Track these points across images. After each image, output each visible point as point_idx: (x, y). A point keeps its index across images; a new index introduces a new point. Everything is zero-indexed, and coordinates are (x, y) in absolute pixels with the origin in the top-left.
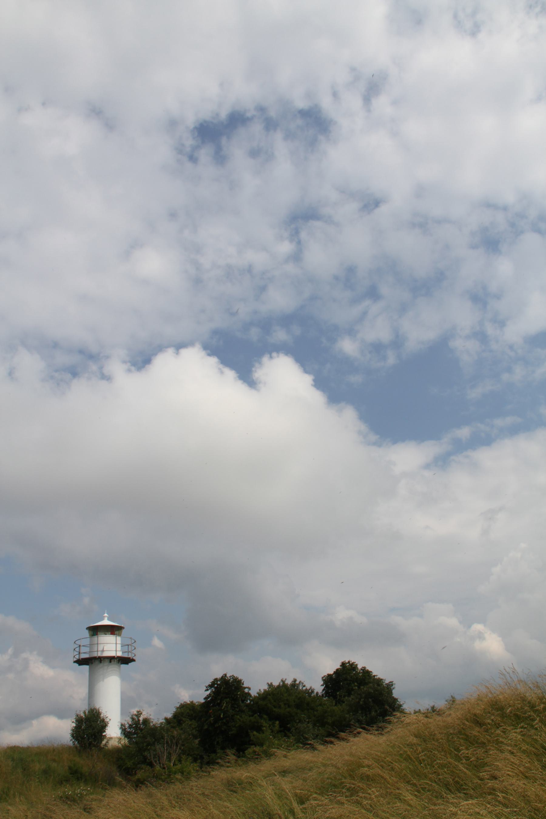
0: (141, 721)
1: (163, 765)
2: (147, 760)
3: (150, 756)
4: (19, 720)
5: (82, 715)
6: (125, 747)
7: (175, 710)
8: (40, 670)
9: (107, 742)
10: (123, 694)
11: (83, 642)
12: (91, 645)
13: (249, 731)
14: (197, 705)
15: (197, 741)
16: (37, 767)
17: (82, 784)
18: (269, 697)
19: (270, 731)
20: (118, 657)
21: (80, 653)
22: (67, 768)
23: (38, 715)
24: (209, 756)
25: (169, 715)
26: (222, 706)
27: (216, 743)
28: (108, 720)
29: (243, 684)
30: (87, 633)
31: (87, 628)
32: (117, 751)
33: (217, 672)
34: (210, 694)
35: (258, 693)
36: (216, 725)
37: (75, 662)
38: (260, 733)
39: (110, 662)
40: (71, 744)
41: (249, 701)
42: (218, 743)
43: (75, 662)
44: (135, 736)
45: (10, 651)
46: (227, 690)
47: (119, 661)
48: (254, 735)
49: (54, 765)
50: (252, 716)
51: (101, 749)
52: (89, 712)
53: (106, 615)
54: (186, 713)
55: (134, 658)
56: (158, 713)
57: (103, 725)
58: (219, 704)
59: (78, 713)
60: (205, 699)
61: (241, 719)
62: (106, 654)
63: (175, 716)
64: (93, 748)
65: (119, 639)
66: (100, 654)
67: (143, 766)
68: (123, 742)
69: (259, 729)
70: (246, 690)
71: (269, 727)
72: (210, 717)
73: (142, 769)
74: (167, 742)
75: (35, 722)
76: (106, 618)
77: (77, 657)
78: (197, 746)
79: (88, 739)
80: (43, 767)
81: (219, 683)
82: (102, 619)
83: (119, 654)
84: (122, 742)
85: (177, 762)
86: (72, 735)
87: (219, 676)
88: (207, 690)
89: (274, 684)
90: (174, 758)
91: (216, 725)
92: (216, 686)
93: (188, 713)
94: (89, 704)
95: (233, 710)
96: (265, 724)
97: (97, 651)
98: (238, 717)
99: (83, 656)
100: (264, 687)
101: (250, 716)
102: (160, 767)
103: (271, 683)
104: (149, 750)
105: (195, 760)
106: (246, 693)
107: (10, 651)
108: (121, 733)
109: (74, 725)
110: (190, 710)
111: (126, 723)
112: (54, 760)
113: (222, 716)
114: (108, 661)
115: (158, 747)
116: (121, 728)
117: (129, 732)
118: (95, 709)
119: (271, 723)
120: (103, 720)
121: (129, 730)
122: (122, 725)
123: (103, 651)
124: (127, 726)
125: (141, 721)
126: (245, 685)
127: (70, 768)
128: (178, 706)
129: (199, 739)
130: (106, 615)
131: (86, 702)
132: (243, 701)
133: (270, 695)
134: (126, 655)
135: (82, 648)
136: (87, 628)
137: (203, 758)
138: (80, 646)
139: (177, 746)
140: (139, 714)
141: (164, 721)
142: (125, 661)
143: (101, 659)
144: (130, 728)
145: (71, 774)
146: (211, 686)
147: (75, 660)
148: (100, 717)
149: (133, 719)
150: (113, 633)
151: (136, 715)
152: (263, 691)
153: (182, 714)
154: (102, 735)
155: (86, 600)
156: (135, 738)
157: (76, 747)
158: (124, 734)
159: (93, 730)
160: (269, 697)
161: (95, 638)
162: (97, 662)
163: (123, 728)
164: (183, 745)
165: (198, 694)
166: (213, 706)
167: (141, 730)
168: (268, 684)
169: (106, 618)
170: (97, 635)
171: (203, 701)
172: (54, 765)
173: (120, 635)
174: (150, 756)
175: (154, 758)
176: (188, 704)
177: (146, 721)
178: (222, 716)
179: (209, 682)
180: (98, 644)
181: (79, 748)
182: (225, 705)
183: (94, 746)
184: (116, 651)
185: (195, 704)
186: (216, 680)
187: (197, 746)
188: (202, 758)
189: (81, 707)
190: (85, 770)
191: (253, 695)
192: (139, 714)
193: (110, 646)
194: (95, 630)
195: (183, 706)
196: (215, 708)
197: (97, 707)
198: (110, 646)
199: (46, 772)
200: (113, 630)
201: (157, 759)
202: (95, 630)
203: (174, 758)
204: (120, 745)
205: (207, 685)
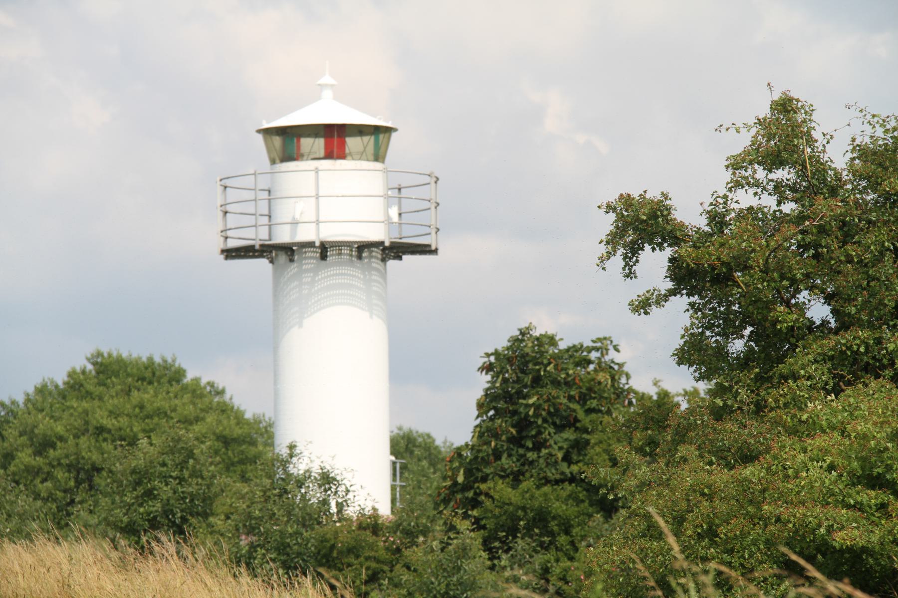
62: (305, 234)
76: (328, 94)
99: (232, 244)
123: (295, 223)
143: (289, 251)
162: (310, 260)
169: (328, 94)
180: (317, 197)
193: (339, 200)
194: (287, 141)
198: (339, 200)
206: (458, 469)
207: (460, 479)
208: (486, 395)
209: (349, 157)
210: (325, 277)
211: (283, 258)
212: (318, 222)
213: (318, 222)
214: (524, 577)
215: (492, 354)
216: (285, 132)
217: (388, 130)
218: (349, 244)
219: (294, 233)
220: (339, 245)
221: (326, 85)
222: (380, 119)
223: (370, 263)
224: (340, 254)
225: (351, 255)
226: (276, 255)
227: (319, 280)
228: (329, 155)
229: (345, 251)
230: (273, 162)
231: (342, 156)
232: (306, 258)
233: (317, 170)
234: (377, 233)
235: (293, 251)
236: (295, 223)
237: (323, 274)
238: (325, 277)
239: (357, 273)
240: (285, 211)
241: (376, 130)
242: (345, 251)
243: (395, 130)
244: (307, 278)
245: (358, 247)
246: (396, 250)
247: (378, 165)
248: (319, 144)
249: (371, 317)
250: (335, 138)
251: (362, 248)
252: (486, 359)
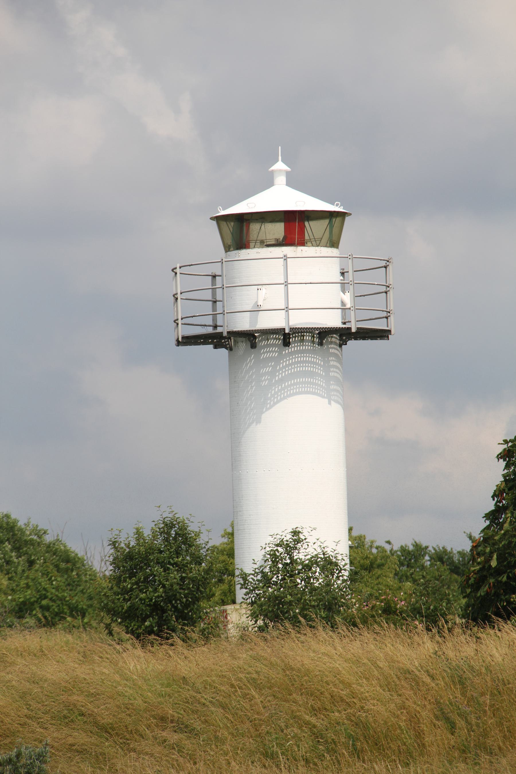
53: (280, 166)
62: (299, 320)
76: (281, 180)
82: (268, 182)
114: (276, 341)
123: (257, 310)
130: (280, 166)
143: (250, 338)
162: (270, 350)
169: (281, 180)
180: (286, 284)
194: (239, 231)
198: (295, 288)
202: (239, 231)
206: (491, 553)
207: (494, 563)
208: (506, 481)
209: (309, 244)
210: (287, 366)
211: (243, 346)
212: (287, 309)
213: (287, 309)
215: (511, 441)
216: (243, 220)
217: (342, 215)
218: (310, 330)
219: (254, 320)
220: (299, 332)
221: (280, 171)
222: (337, 205)
223: (328, 348)
224: (302, 341)
225: (313, 342)
226: (235, 341)
227: (281, 369)
228: (287, 241)
229: (308, 338)
230: (227, 249)
231: (302, 243)
233: (285, 258)
234: (334, 321)
235: (255, 337)
236: (257, 310)
238: (287, 366)
239: (318, 360)
240: (244, 299)
241: (331, 215)
242: (308, 338)
243: (350, 214)
245: (319, 334)
246: (344, 335)
247: (333, 252)
248: (278, 230)
249: (330, 403)
250: (294, 227)
251: (323, 335)
252: (505, 446)
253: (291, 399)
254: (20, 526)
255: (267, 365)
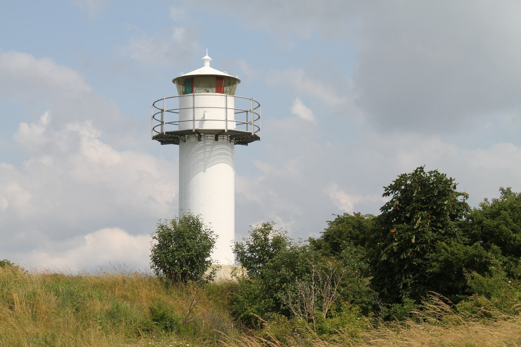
0: (270, 242)
1: (309, 314)
2: (282, 307)
3: (287, 299)
4: (64, 234)
5: (170, 226)
6: (244, 283)
7: (327, 227)
8: (97, 153)
9: (213, 273)
10: (238, 196)
11: (165, 105)
12: (183, 109)
13: (464, 269)
14: (367, 221)
15: (367, 281)
16: (98, 307)
17: (172, 338)
18: (503, 212)
19: (504, 274)
20: (229, 131)
21: (162, 122)
22: (147, 311)
23: (94, 226)
24: (389, 307)
25: (318, 236)
26: (414, 224)
27: (401, 287)
28: (214, 237)
29: (455, 187)
30: (174, 89)
31: (174, 81)
32: (231, 288)
33: (407, 161)
34: (392, 201)
35: (482, 205)
36: (403, 256)
37: (155, 138)
38: (484, 276)
39: (216, 139)
40: (152, 272)
41: (464, 218)
42: (405, 285)
43: (155, 138)
44: (261, 265)
45: (45, 119)
46: (423, 197)
47: (231, 138)
48: (473, 278)
49: (126, 304)
50: (470, 245)
51: (203, 284)
52: (181, 222)
53: (207, 57)
54: (345, 234)
55: (257, 134)
56: (300, 228)
57: (206, 245)
58: (408, 220)
59: (163, 223)
60: (382, 209)
61: (449, 249)
62: (208, 126)
63: (327, 237)
64: (190, 281)
65: (231, 100)
66: (197, 126)
67: (275, 315)
68: (239, 274)
69: (483, 268)
70: (460, 199)
71: (503, 266)
72: (392, 240)
73: (274, 319)
74: (316, 279)
75: (88, 238)
76: (207, 64)
77: (158, 129)
78: (368, 288)
79: (181, 266)
80: (108, 307)
81: (409, 182)
82: (202, 65)
83: (232, 126)
84: (238, 275)
85: (333, 313)
86: (154, 259)
87: (410, 170)
88: (387, 194)
89: (513, 191)
90: (328, 305)
91: (403, 256)
92: (403, 187)
93: (350, 232)
94: (181, 210)
95: (434, 231)
96: (496, 259)
97: (194, 120)
98: (444, 244)
99: (168, 128)
100: (493, 195)
101: (465, 245)
102: (305, 318)
103: (509, 189)
104: (284, 289)
105: (365, 312)
106: (460, 204)
107: (45, 119)
108: (237, 259)
109: (157, 242)
110: (354, 227)
111: (244, 243)
112: (125, 298)
113: (413, 241)
114: (212, 137)
115: (300, 285)
116: (236, 251)
117: (250, 258)
118: (191, 217)
119: (506, 259)
120: (206, 237)
121: (249, 255)
122: (237, 246)
123: (203, 120)
124: (247, 247)
125: (270, 242)
126: (458, 190)
127: (152, 311)
128: (333, 220)
129: (371, 278)
130: (207, 57)
131: (177, 207)
132: (453, 217)
133: (505, 210)
134: (242, 129)
135: (165, 113)
136: (174, 81)
137: (379, 310)
138: (163, 110)
139: (333, 285)
140: (267, 228)
141: (308, 243)
142: (242, 138)
143: (199, 134)
144: (251, 252)
145: (154, 320)
146: (394, 187)
147: (155, 134)
148: (200, 232)
149: (256, 237)
150: (219, 90)
151: (261, 230)
152: (491, 202)
153: (340, 234)
154: (204, 261)
155: (178, 34)
156: (260, 268)
157: (161, 279)
158: (242, 260)
159: (188, 251)
160: (503, 212)
161: (189, 98)
162: (193, 139)
163: (239, 250)
164: (343, 286)
165: (371, 203)
166: (399, 222)
167: (271, 256)
168: (502, 189)
169: (207, 64)
170: (192, 92)
171: (378, 213)
172: (126, 304)
173: (232, 93)
174: (287, 299)
175: (293, 303)
176: (351, 217)
177: (278, 242)
178: (413, 241)
179: (390, 181)
180: (194, 108)
181: (165, 280)
182: (419, 221)
183: (191, 278)
184: (226, 121)
185: (363, 218)
186: (404, 177)
187: (368, 288)
188: (376, 309)
189: (168, 215)
190: (177, 315)
191: (472, 208)
192: (267, 228)
193: (214, 111)
194: (189, 84)
195: (341, 221)
196: (400, 226)
197: (195, 215)
198: (214, 111)
199: (112, 315)
200: (220, 83)
201: (298, 306)
202: (189, 84)
203: (328, 305)
204: (234, 278)
205: (387, 185)
214: (409, 254)
219: (201, 125)
226: (188, 137)
227: (214, 150)
232: (207, 139)
237: (216, 147)
244: (208, 149)
253: (216, 165)
254: (475, 209)
255: (202, 150)
